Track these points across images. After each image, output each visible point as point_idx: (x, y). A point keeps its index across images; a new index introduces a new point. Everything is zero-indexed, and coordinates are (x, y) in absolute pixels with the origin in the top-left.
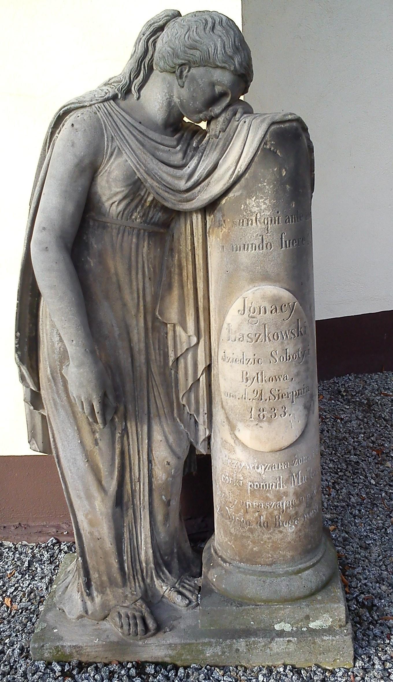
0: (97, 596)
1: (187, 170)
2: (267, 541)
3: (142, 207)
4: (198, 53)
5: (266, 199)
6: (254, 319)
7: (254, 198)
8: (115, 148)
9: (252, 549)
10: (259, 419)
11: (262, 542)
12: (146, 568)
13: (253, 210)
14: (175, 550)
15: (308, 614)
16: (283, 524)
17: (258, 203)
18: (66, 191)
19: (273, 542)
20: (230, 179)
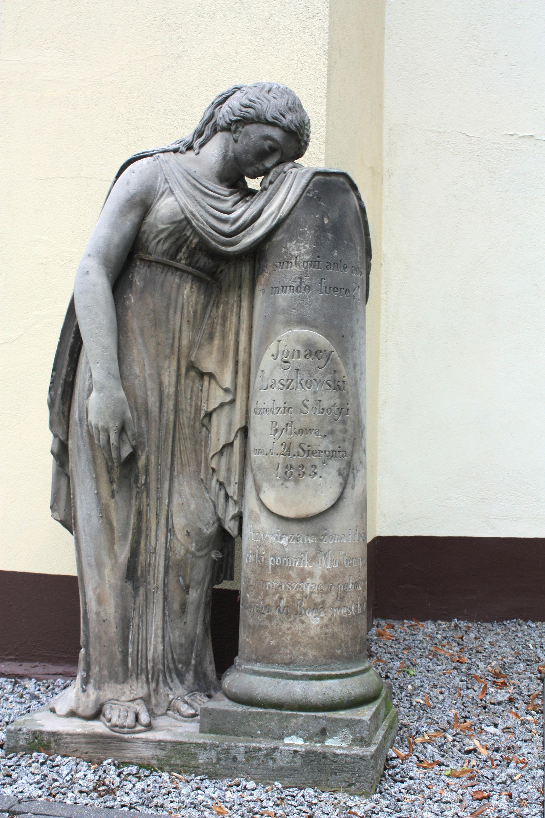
0: (93, 693)
1: (234, 215)
2: (287, 632)
3: (188, 247)
4: (252, 111)
5: (306, 244)
6: (287, 364)
7: (295, 241)
8: (166, 190)
9: (269, 643)
10: (286, 478)
11: (280, 634)
12: (153, 667)
13: (293, 253)
14: (193, 662)
15: (324, 725)
16: (305, 612)
17: (299, 246)
18: (115, 223)
19: (293, 634)
20: (272, 222)
